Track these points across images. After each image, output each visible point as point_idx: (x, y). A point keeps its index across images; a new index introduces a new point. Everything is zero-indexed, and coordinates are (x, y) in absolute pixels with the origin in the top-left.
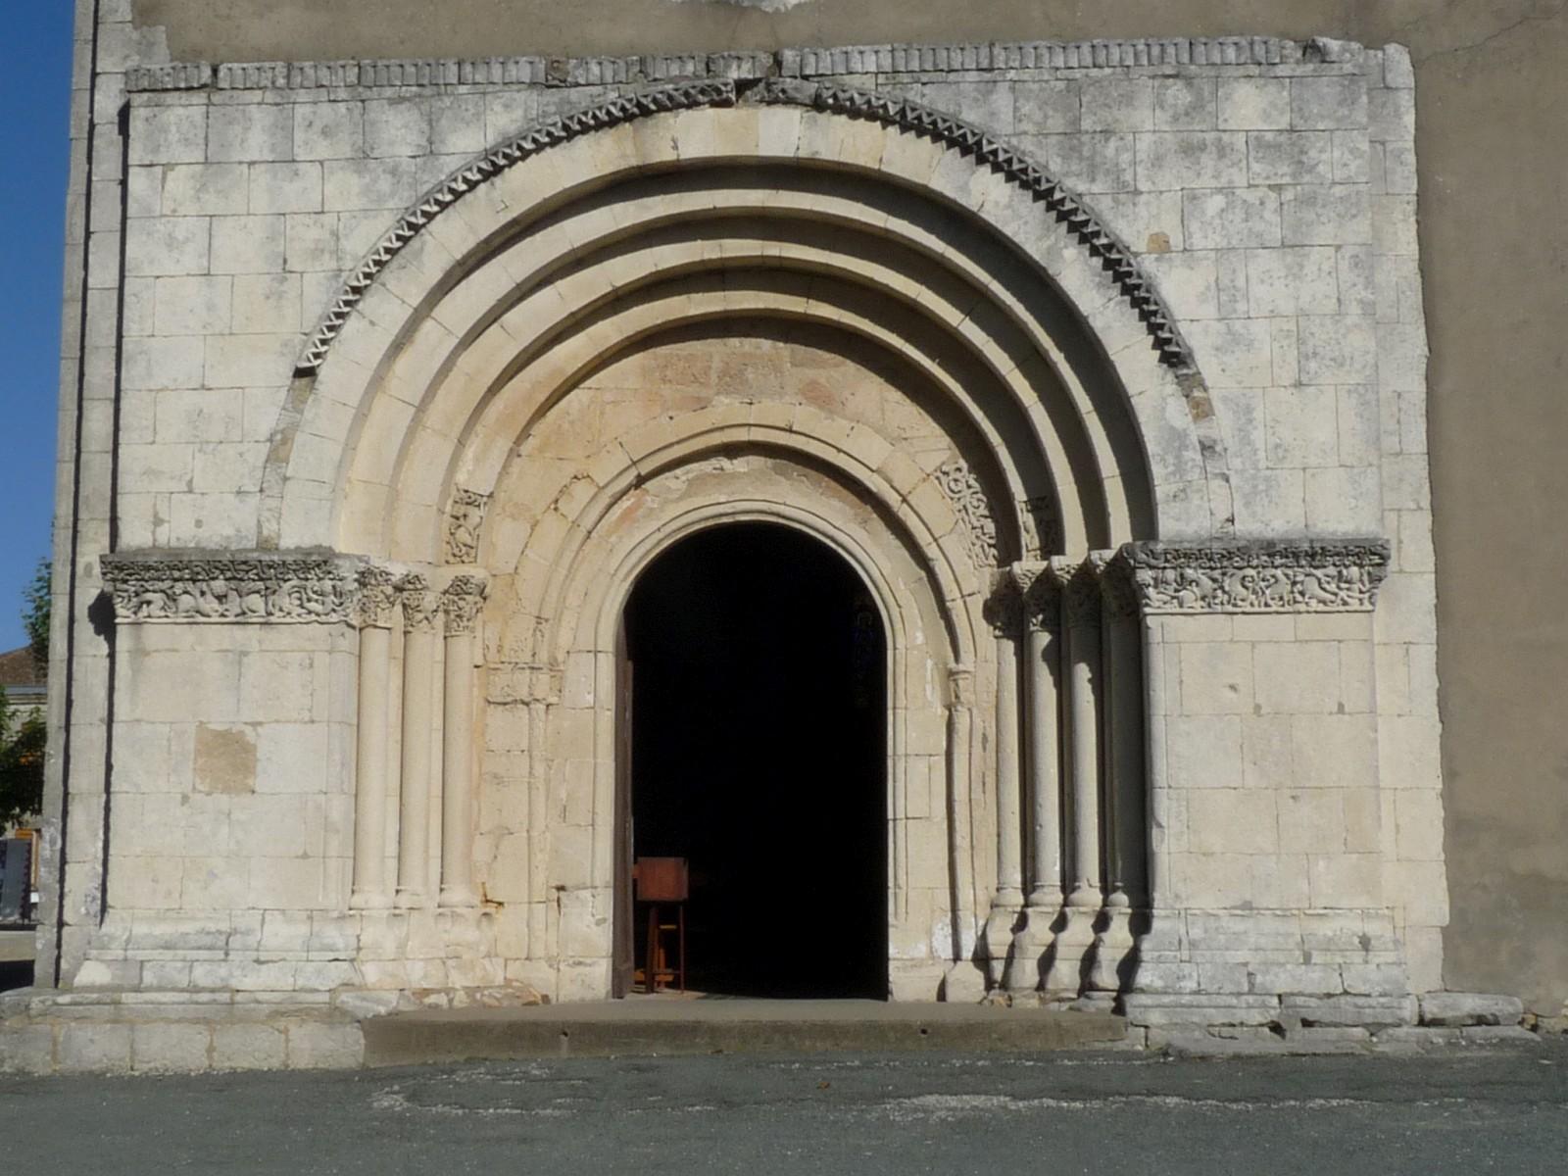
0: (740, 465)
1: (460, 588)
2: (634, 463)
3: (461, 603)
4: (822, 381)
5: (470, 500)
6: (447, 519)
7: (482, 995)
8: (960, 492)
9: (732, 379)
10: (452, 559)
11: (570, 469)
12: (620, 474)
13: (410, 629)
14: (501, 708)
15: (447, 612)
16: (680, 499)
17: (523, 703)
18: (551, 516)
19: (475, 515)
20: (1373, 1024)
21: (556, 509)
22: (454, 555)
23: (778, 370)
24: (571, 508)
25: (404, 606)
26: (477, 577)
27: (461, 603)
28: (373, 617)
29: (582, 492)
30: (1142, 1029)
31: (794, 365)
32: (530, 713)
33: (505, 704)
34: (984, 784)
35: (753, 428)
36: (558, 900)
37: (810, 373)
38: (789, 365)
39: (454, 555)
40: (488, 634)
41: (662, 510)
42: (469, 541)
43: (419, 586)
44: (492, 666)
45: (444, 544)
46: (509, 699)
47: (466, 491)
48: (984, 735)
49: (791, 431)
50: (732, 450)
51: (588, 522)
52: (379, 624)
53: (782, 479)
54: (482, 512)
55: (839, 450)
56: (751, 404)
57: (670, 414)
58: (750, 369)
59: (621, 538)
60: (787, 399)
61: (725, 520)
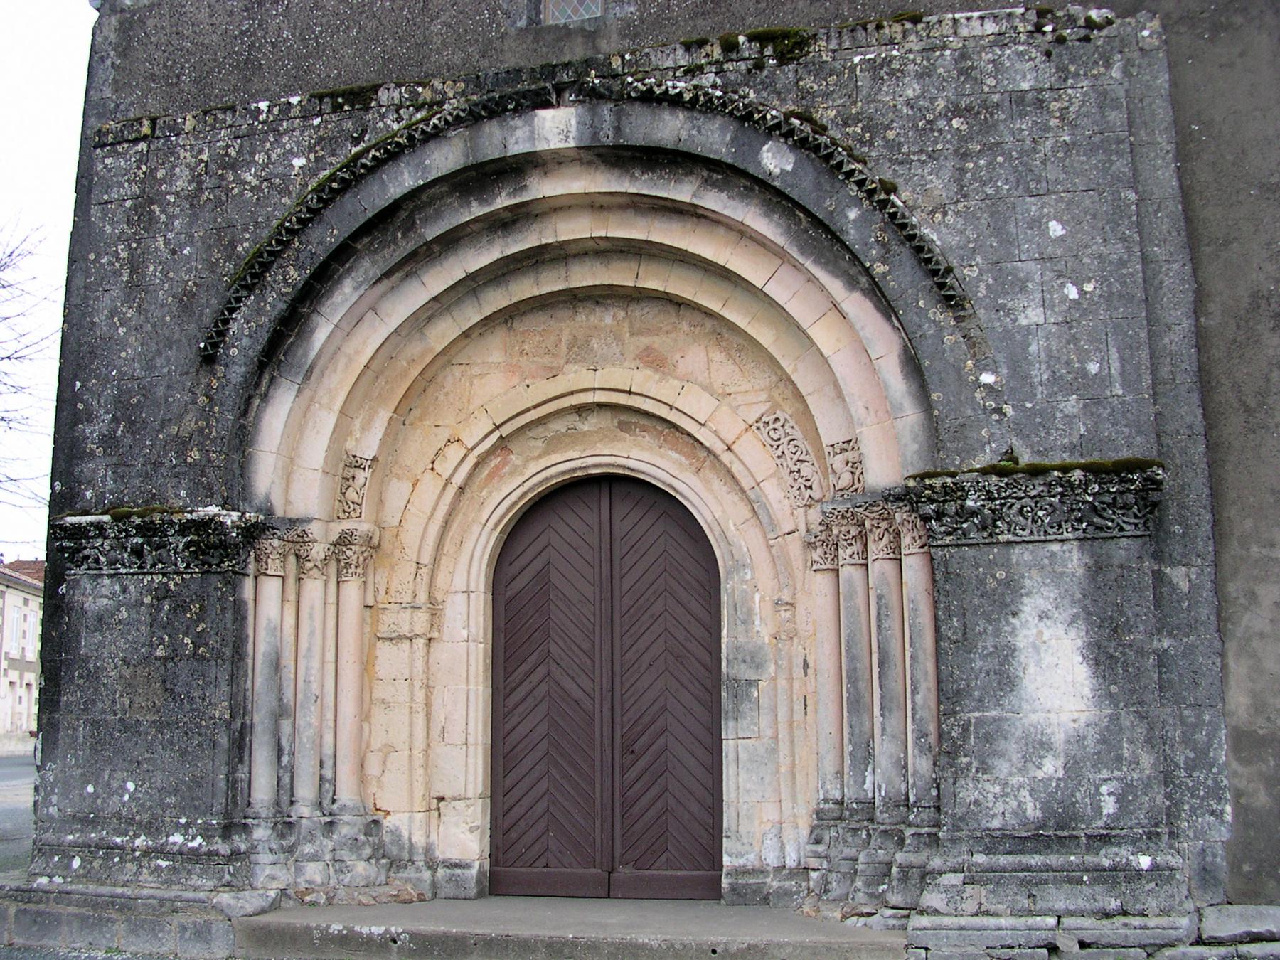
0: (590, 424)
1: (344, 541)
2: (498, 427)
3: (349, 553)
4: (656, 346)
5: (356, 464)
6: (338, 479)
7: (360, 894)
8: (779, 439)
9: (579, 351)
10: (342, 515)
11: (445, 434)
12: (486, 436)
13: (302, 576)
14: (388, 643)
15: (338, 561)
16: (539, 457)
17: (407, 638)
18: (429, 474)
19: (361, 476)
20: (1151, 945)
21: (432, 469)
22: (344, 511)
23: (618, 338)
24: (445, 468)
25: (298, 557)
26: (360, 529)
27: (349, 553)
28: (265, 566)
29: (455, 453)
30: (923, 951)
31: (632, 334)
32: (411, 646)
33: (391, 639)
34: (805, 705)
35: (597, 392)
36: (438, 809)
37: (645, 341)
38: (628, 334)
39: (344, 511)
40: (378, 578)
41: (525, 466)
42: (356, 500)
43: (307, 540)
44: (381, 606)
45: (337, 502)
46: (393, 635)
47: (354, 456)
48: (805, 661)
49: (630, 392)
50: (581, 410)
51: (459, 479)
52: (268, 572)
53: (627, 435)
54: (368, 473)
55: (671, 407)
56: (595, 370)
57: (527, 382)
58: (594, 340)
59: (490, 493)
60: (626, 364)
61: (579, 474)
